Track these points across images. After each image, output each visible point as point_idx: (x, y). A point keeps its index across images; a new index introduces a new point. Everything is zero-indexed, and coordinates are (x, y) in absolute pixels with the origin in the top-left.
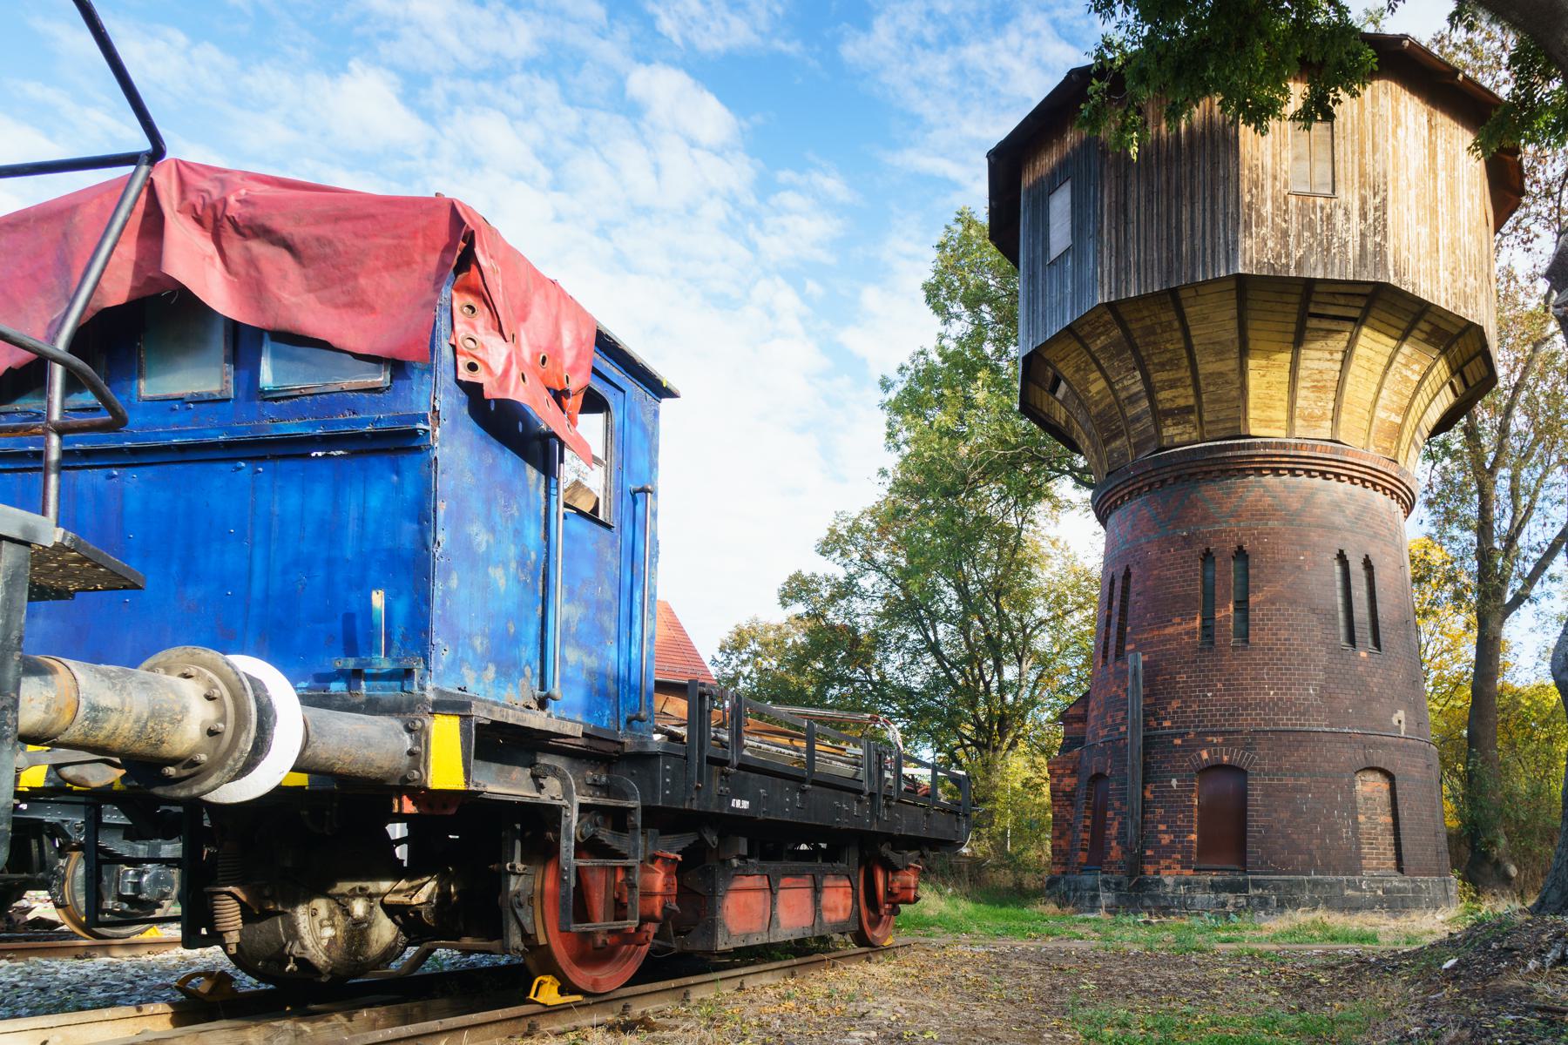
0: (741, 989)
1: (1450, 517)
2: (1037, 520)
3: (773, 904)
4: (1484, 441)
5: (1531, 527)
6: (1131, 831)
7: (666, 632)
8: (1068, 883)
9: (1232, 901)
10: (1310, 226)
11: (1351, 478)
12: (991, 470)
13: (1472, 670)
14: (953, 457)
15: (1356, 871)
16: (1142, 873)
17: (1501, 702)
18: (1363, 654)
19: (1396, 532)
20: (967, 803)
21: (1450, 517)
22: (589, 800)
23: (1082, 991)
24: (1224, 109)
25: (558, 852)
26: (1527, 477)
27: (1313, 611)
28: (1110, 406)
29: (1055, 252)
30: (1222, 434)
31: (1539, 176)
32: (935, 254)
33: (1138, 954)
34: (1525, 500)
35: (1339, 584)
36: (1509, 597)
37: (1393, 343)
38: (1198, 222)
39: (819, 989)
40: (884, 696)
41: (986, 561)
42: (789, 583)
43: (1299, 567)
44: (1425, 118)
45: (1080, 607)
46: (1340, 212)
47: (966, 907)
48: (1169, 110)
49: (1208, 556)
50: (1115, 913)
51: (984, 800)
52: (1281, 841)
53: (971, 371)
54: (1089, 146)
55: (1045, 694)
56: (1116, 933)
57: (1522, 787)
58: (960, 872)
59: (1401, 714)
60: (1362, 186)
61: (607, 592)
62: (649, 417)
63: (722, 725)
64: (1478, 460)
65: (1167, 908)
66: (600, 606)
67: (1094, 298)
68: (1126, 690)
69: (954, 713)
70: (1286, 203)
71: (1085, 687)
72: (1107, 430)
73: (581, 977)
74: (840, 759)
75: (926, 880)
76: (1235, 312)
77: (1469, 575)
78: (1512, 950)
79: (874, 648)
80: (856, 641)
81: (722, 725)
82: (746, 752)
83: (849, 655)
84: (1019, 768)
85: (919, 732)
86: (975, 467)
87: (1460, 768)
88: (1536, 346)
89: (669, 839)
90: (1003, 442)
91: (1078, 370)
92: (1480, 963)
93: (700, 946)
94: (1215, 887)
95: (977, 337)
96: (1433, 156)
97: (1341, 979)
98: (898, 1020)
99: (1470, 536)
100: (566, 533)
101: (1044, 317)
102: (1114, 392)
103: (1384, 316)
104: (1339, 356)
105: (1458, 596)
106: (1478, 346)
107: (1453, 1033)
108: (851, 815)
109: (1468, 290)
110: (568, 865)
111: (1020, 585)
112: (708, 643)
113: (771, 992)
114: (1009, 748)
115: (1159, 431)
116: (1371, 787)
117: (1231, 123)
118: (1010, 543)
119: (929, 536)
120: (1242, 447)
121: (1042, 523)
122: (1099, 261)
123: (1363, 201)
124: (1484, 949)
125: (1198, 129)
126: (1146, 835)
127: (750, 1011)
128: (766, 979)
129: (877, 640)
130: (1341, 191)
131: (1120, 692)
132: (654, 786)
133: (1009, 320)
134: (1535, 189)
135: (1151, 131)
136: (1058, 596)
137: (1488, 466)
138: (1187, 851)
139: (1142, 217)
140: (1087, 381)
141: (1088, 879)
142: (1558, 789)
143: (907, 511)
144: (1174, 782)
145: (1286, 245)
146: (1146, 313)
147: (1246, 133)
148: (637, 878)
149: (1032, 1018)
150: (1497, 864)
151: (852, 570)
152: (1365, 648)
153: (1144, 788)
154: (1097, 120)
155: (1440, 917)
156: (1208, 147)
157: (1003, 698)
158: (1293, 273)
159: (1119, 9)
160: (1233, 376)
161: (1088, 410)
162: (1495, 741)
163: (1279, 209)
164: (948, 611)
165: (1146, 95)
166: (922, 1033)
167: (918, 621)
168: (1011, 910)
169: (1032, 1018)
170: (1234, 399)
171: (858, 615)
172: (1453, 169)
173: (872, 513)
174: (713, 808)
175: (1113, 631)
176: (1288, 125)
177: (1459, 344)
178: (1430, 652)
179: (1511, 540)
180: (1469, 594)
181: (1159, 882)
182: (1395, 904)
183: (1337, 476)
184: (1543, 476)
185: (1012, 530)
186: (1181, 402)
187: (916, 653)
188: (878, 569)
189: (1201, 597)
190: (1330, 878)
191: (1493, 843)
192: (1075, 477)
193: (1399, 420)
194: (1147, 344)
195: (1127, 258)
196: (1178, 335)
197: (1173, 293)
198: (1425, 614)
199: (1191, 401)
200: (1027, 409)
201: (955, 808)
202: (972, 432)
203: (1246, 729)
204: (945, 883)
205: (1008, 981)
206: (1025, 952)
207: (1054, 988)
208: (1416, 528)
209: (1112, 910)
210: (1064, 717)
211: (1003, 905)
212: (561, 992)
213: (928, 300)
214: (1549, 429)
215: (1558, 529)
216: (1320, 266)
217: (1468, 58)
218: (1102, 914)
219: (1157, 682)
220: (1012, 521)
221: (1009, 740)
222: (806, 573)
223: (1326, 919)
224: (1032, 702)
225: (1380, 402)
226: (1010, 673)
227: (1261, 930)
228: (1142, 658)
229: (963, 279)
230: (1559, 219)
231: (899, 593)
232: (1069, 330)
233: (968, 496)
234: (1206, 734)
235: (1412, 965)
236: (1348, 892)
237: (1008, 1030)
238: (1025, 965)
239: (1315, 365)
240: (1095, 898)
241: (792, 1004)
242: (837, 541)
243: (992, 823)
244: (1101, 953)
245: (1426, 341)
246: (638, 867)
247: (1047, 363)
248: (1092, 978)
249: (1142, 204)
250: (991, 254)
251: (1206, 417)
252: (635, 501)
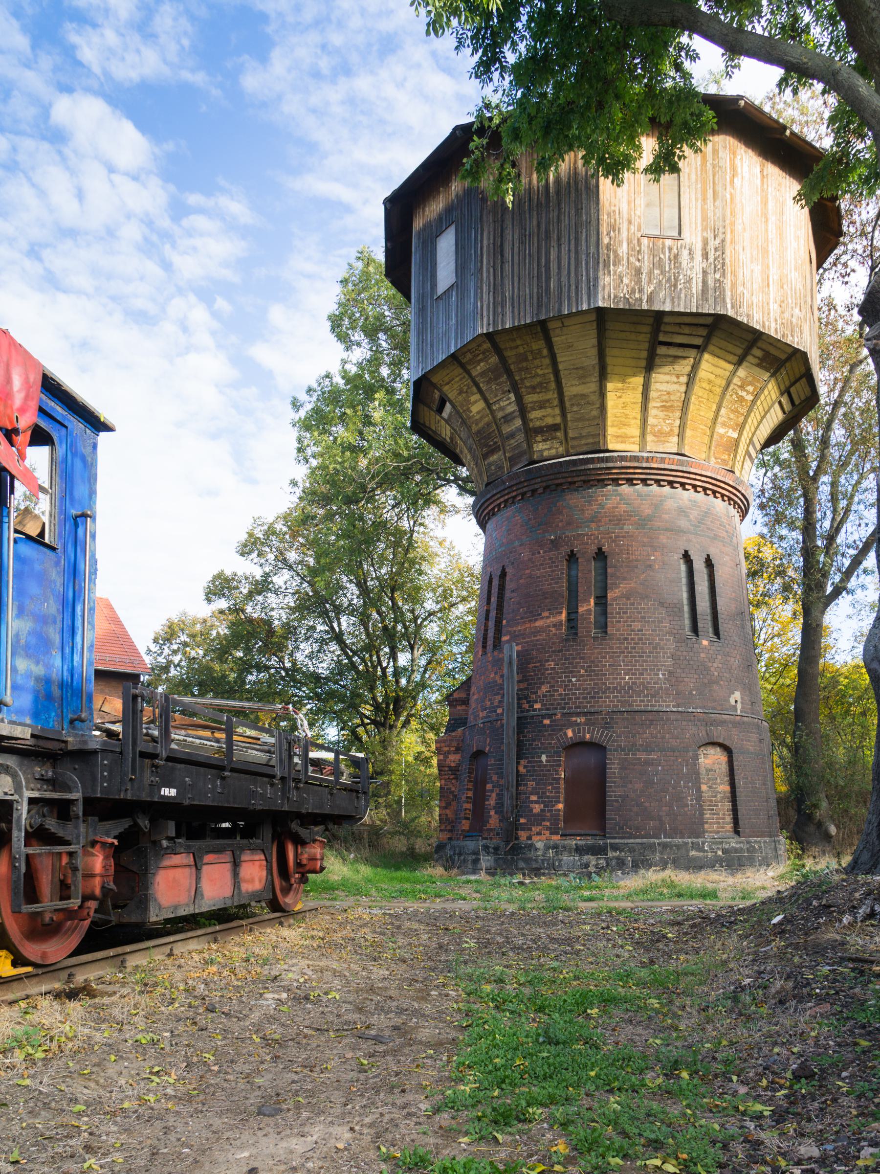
0: (170, 955)
1: (779, 519)
2: (427, 522)
3: (198, 879)
4: (809, 450)
5: (848, 527)
6: (507, 802)
7: (106, 625)
8: (453, 848)
9: (594, 863)
10: (660, 264)
11: (695, 487)
12: (386, 481)
13: (798, 652)
14: (354, 469)
15: (699, 834)
16: (517, 838)
17: (822, 682)
18: (705, 642)
19: (733, 534)
20: (368, 781)
21: (779, 519)
22: (36, 794)
23: (465, 949)
24: (586, 162)
25: (10, 840)
26: (845, 482)
27: (662, 604)
28: (488, 424)
29: (442, 287)
30: (585, 449)
31: (855, 217)
32: (338, 289)
33: (513, 914)
34: (843, 504)
35: (684, 581)
36: (829, 589)
37: (730, 367)
38: (565, 262)
39: (239, 953)
40: (295, 681)
41: (382, 559)
42: (213, 581)
43: (650, 566)
44: (758, 169)
45: (464, 599)
46: (685, 253)
47: (366, 870)
48: (539, 164)
49: (572, 557)
50: (493, 875)
51: (381, 773)
52: (635, 809)
53: (370, 392)
54: (471, 196)
55: (434, 677)
56: (495, 893)
57: (841, 754)
58: (361, 839)
59: (737, 695)
60: (704, 229)
61: (51, 607)
62: (89, 449)
63: (152, 722)
64: (803, 468)
65: (538, 869)
66: (43, 620)
67: (475, 329)
68: (502, 676)
69: (355, 695)
70: (640, 244)
71: (469, 672)
72: (486, 445)
73: (32, 950)
74: (253, 743)
75: (331, 847)
76: (595, 341)
77: (795, 570)
78: (830, 906)
79: (287, 639)
80: (271, 632)
81: (152, 722)
82: (173, 746)
83: (265, 645)
84: (411, 743)
85: (325, 713)
86: (373, 478)
87: (789, 739)
88: (853, 367)
89: (107, 825)
90: (397, 455)
91: (461, 392)
92: (803, 918)
93: (134, 919)
94: (579, 850)
95: (374, 362)
96: (765, 203)
97: (686, 934)
98: (305, 981)
99: (797, 535)
100: (17, 556)
101: (432, 346)
102: (492, 412)
103: (723, 344)
104: (684, 379)
105: (786, 588)
106: (803, 370)
107: (779, 984)
108: (265, 797)
109: (794, 320)
110: (19, 853)
111: (412, 581)
112: (143, 635)
113: (196, 957)
114: (403, 726)
115: (530, 446)
116: (712, 760)
117: (592, 176)
118: (403, 544)
119: (333, 538)
120: (601, 460)
121: (431, 526)
122: (479, 295)
123: (705, 243)
124: (808, 903)
125: (564, 179)
126: (520, 806)
127: (178, 976)
128: (193, 945)
129: (289, 630)
130: (685, 234)
131: (497, 678)
132: (94, 779)
133: (403, 346)
134: (852, 230)
135: (524, 180)
136: (445, 591)
137: (811, 473)
138: (555, 819)
139: (516, 257)
140: (468, 402)
141: (470, 845)
142: (869, 756)
143: (314, 518)
144: (544, 758)
145: (639, 281)
146: (519, 342)
147: (605, 184)
148: (80, 862)
149: (421, 975)
150: (820, 825)
151: (267, 569)
152: (707, 637)
153: (518, 763)
154: (477, 172)
155: (771, 874)
156: (573, 195)
157: (397, 682)
158: (645, 306)
159: (496, 75)
160: (594, 398)
161: (469, 428)
162: (818, 715)
163: (633, 249)
164: (350, 605)
165: (519, 151)
166: (326, 993)
167: (324, 614)
168: (404, 873)
169: (421, 975)
170: (595, 418)
171: (272, 609)
172: (782, 213)
173: (285, 517)
174: (145, 797)
175: (491, 624)
176: (642, 179)
177: (787, 366)
178: (763, 636)
179: (831, 538)
180: (796, 586)
181: (531, 847)
182: (733, 862)
183: (683, 485)
184: (858, 482)
185: (405, 532)
186: (550, 421)
187: (323, 642)
188: (290, 568)
189: (566, 594)
190: (678, 841)
191: (816, 806)
192: (459, 486)
193: (735, 435)
194: (521, 370)
195: (503, 293)
196: (547, 361)
197: (543, 324)
198: (758, 605)
199: (558, 420)
200: (417, 427)
201: (355, 787)
202: (370, 447)
203: (605, 710)
204: (348, 849)
205: (401, 941)
206: (416, 913)
207: (441, 947)
208: (751, 529)
209: (491, 872)
210: (450, 699)
211: (398, 869)
212: (14, 964)
213: (333, 330)
214: (864, 440)
215: (871, 529)
216: (668, 300)
217: (796, 113)
218: (482, 876)
219: (528, 669)
220: (405, 524)
221: (402, 719)
222: (228, 572)
223: (674, 878)
224: (422, 685)
225: (720, 420)
226: (403, 659)
227: (618, 888)
228: (516, 648)
229: (363, 311)
230: (872, 256)
231: (308, 589)
232: (453, 356)
233: (367, 502)
234: (571, 714)
235: (746, 921)
236: (693, 853)
237: (400, 988)
238: (415, 926)
239: (664, 387)
240: (476, 861)
241: (214, 969)
242: (254, 544)
243: (389, 793)
244: (481, 913)
245: (758, 365)
246: (80, 852)
247: (434, 386)
248: (473, 937)
249: (516, 250)
250: (387, 289)
251: (571, 434)
252: (76, 526)
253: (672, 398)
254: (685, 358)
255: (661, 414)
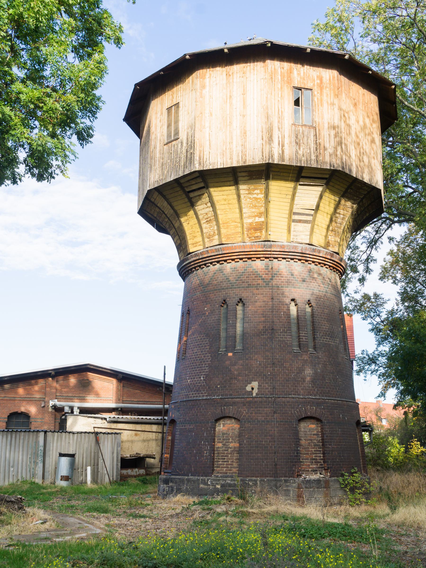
37: (233, 188)
104: (209, 204)
236: (201, 486)
239: (203, 212)
245: (251, 179)
253: (209, 215)
254: (203, 194)
255: (208, 226)
